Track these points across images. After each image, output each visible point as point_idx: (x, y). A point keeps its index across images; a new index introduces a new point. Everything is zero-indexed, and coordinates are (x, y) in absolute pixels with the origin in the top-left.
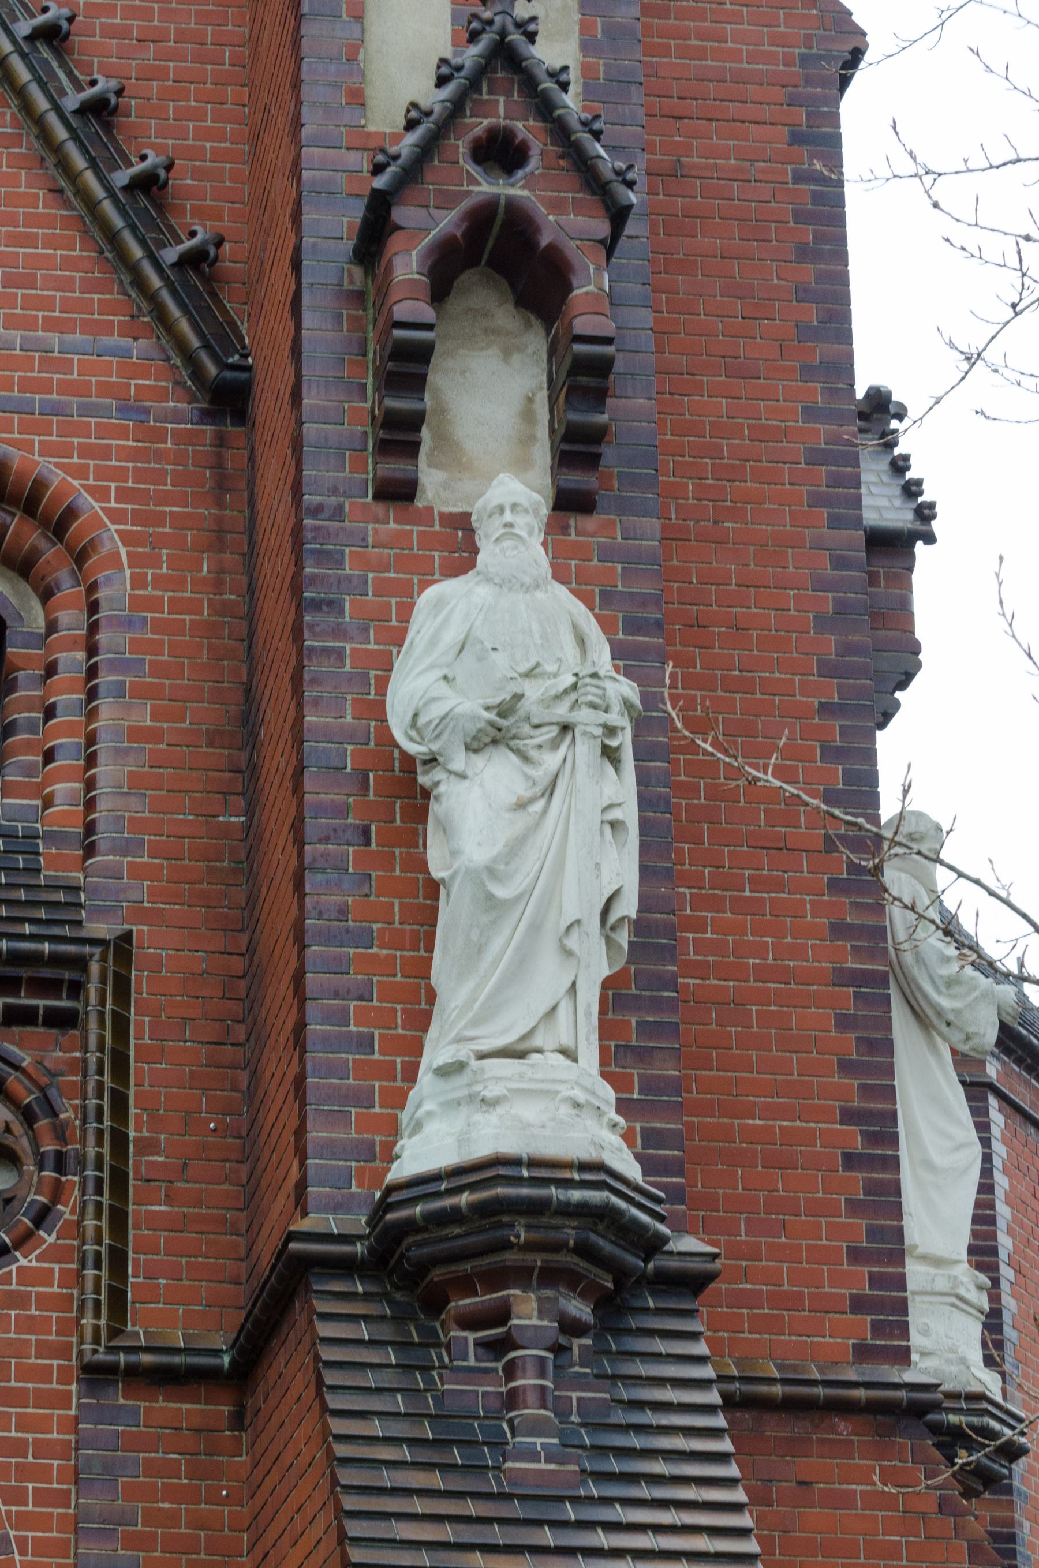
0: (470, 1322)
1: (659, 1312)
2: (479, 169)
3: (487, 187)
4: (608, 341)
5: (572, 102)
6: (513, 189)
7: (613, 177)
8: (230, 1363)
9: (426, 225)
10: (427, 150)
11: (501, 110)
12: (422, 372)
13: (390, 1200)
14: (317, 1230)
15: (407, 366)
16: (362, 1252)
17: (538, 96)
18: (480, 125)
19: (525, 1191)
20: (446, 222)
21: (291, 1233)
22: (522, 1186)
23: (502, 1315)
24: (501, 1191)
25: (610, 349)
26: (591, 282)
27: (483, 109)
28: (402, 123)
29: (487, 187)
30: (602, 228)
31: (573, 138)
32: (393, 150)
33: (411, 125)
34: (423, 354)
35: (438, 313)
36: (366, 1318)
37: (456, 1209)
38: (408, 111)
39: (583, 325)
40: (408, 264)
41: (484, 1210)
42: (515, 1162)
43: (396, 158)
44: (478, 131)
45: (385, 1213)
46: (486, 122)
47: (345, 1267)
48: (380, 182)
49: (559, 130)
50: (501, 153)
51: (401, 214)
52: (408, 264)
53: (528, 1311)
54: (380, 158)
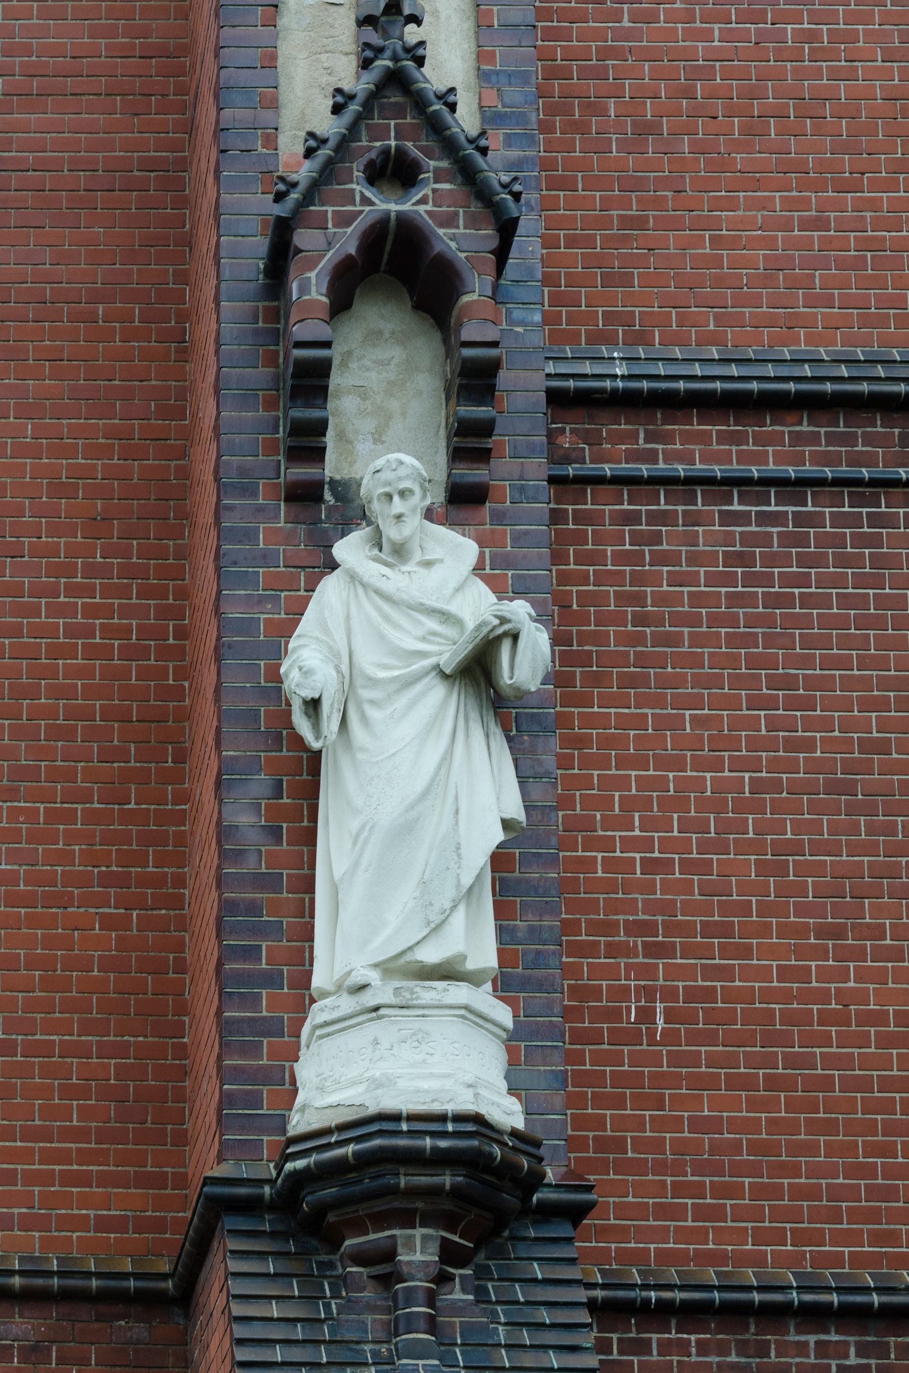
0: (360, 1258)
2: (374, 190)
3: (387, 204)
4: (495, 344)
5: (466, 119)
6: (415, 205)
7: (499, 189)
8: (174, 1287)
9: (326, 244)
10: (328, 174)
12: (323, 384)
13: (288, 1151)
14: (225, 1176)
15: (311, 381)
16: (271, 1194)
17: (429, 115)
18: (370, 147)
19: (402, 1142)
20: (347, 241)
21: (206, 1178)
22: (332, 1149)
23: (388, 1255)
24: (377, 1142)
25: (493, 352)
26: (476, 291)
27: (381, 133)
28: (301, 150)
29: (387, 204)
30: (488, 235)
31: (461, 153)
32: (294, 177)
33: (309, 153)
34: (323, 369)
35: (334, 331)
36: (276, 1254)
37: (343, 1160)
38: (306, 140)
39: (469, 333)
40: (311, 285)
41: (365, 1161)
42: (396, 1117)
43: (294, 185)
44: (373, 155)
45: (286, 1162)
47: (249, 1206)
48: (282, 210)
49: (448, 145)
50: (396, 172)
51: (303, 238)
52: (311, 285)
53: (418, 1249)
54: (281, 187)
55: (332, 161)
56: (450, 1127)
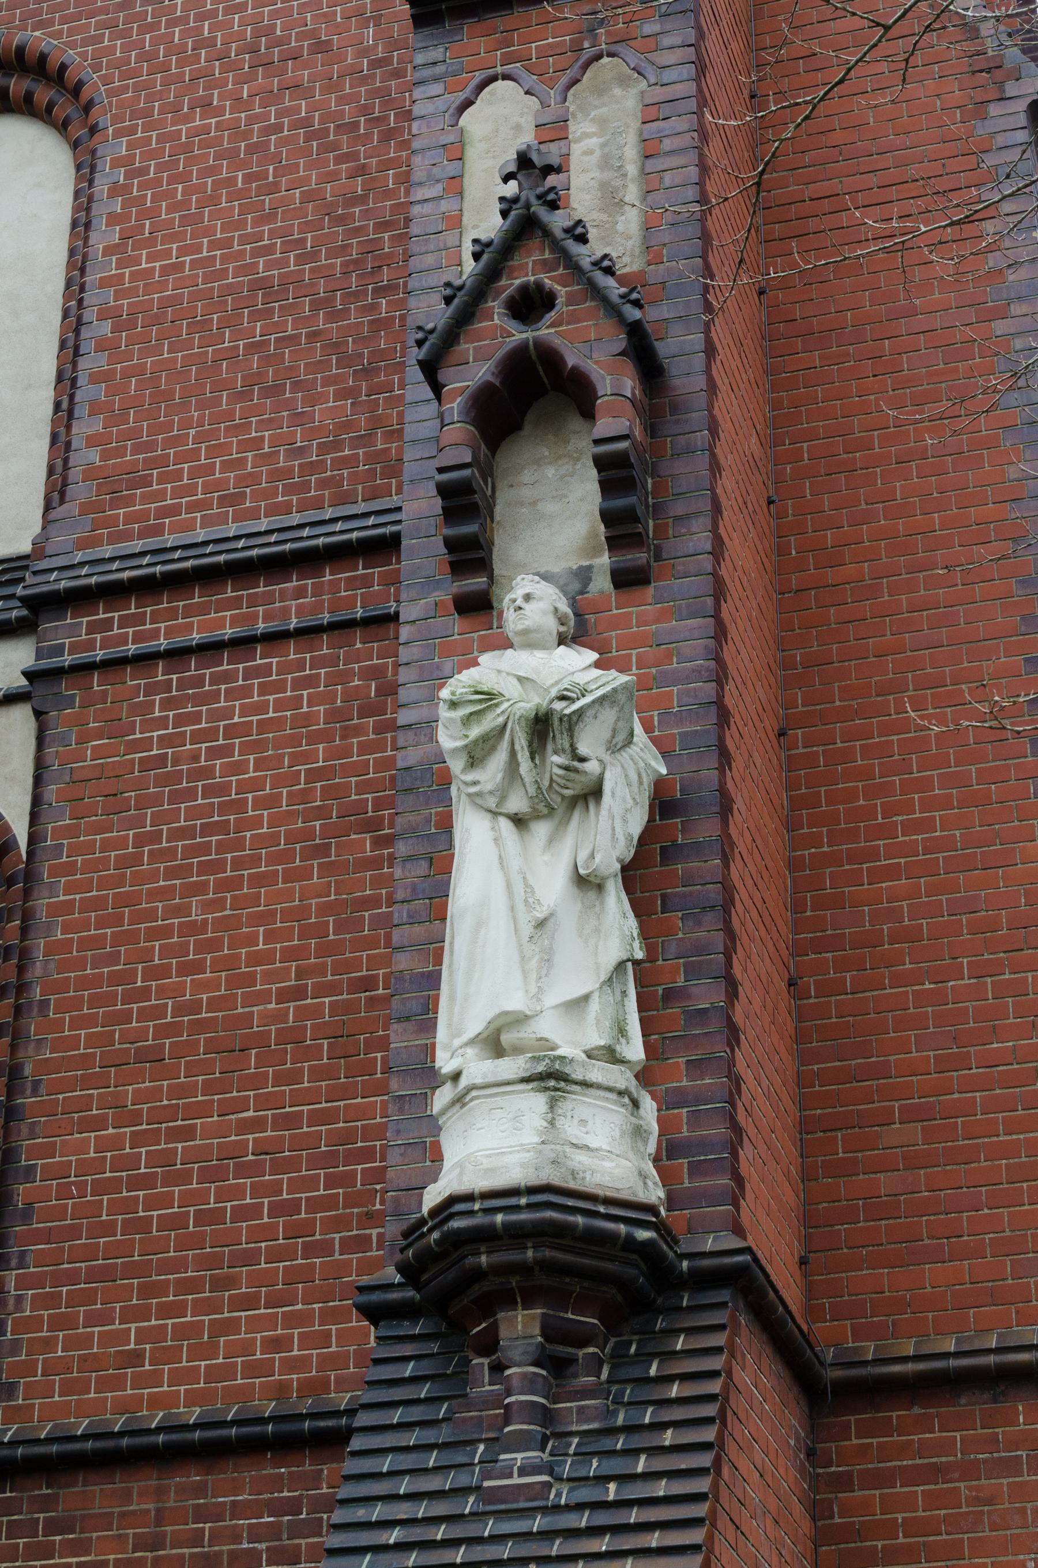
1: (691, 1309)
9: (474, 369)
11: (529, 269)
18: (511, 284)
42: (469, 1198)
46: (517, 282)
55: (467, 306)
56: (523, 1201)
